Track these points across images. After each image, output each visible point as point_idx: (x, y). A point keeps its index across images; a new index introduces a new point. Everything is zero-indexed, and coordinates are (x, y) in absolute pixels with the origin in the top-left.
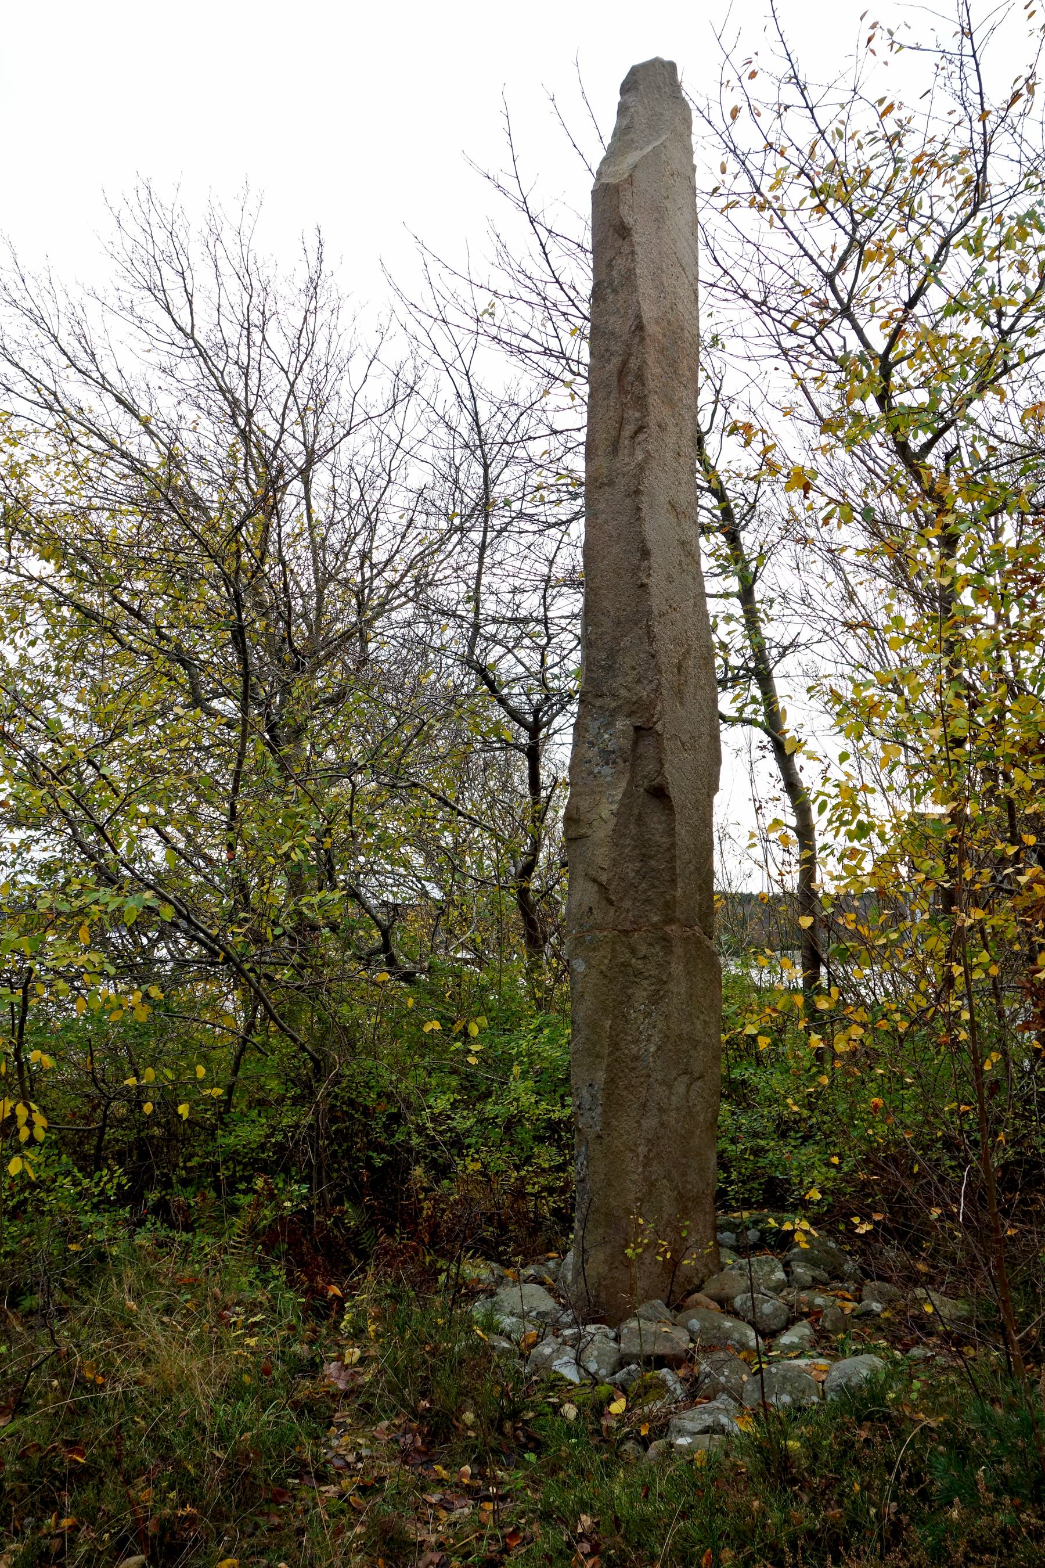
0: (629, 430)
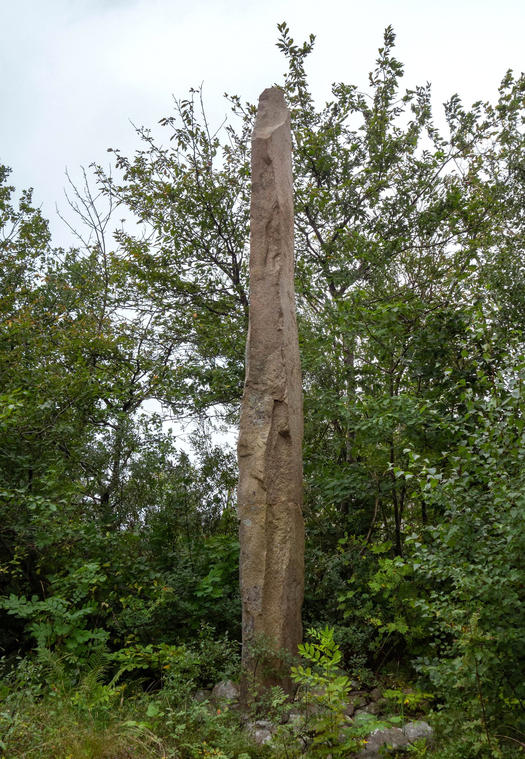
0: (271, 255)
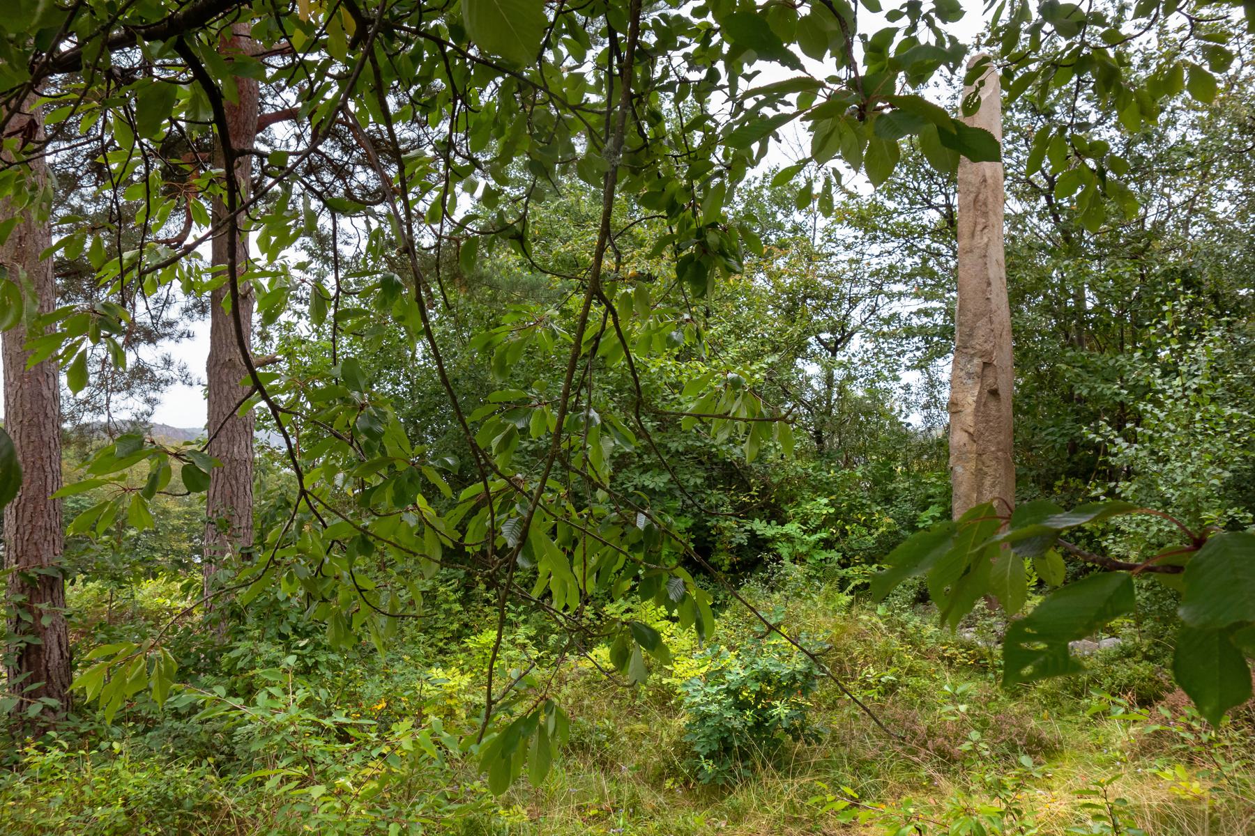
0: (979, 227)
